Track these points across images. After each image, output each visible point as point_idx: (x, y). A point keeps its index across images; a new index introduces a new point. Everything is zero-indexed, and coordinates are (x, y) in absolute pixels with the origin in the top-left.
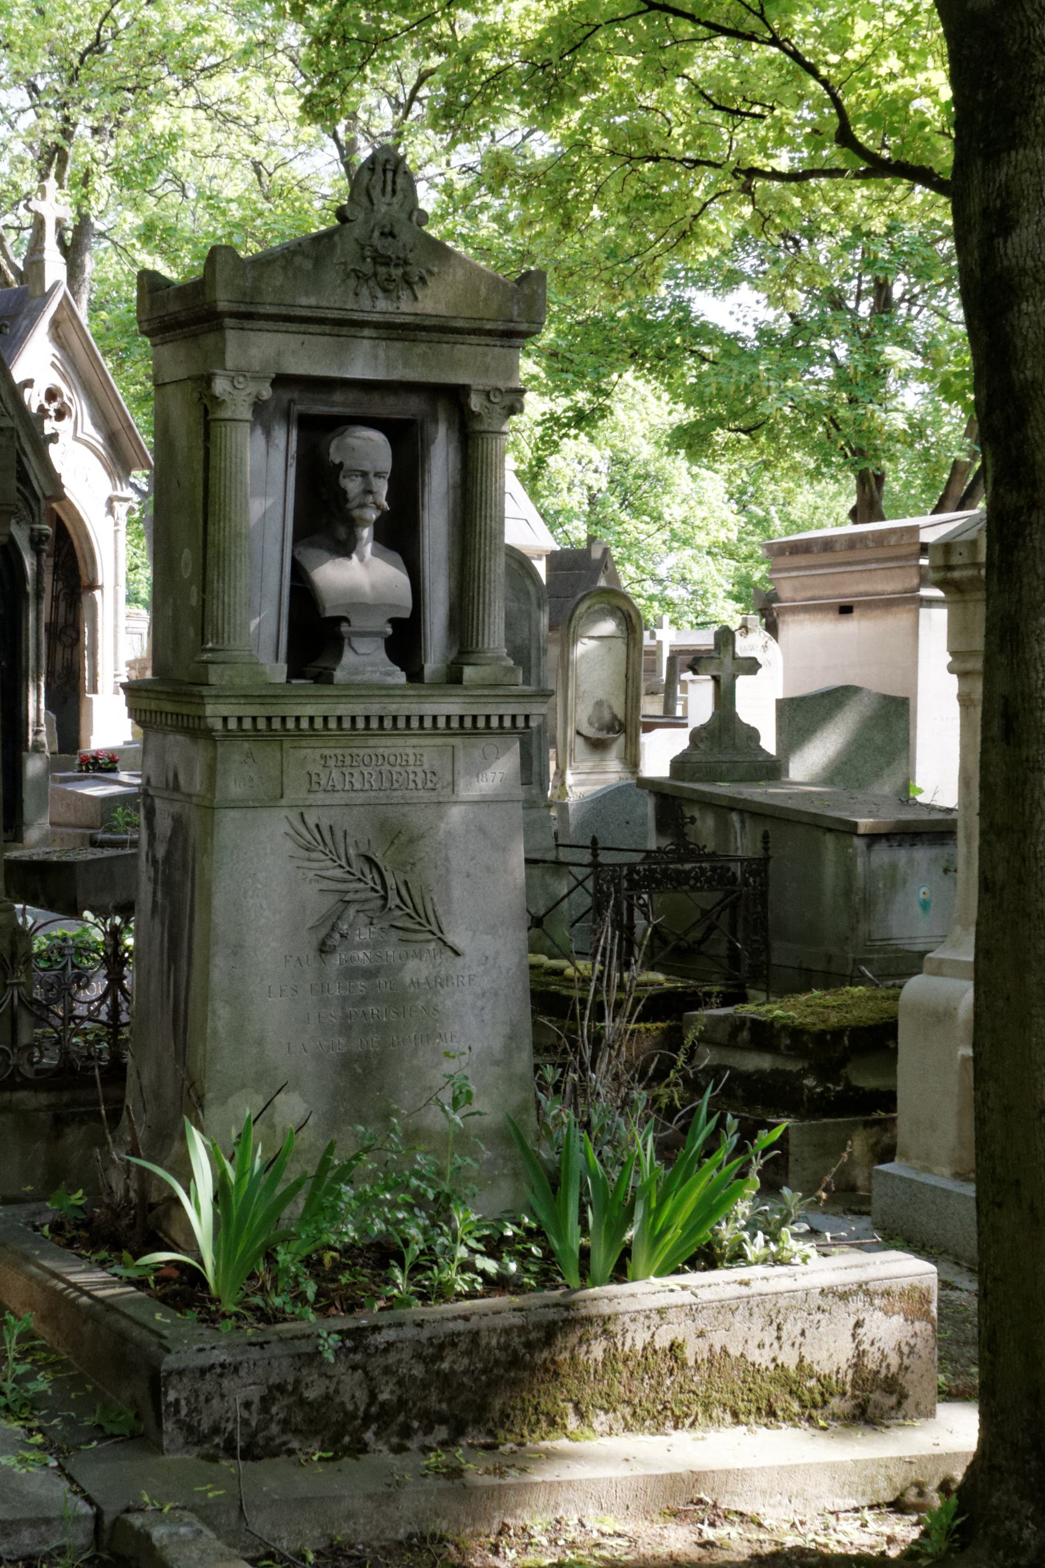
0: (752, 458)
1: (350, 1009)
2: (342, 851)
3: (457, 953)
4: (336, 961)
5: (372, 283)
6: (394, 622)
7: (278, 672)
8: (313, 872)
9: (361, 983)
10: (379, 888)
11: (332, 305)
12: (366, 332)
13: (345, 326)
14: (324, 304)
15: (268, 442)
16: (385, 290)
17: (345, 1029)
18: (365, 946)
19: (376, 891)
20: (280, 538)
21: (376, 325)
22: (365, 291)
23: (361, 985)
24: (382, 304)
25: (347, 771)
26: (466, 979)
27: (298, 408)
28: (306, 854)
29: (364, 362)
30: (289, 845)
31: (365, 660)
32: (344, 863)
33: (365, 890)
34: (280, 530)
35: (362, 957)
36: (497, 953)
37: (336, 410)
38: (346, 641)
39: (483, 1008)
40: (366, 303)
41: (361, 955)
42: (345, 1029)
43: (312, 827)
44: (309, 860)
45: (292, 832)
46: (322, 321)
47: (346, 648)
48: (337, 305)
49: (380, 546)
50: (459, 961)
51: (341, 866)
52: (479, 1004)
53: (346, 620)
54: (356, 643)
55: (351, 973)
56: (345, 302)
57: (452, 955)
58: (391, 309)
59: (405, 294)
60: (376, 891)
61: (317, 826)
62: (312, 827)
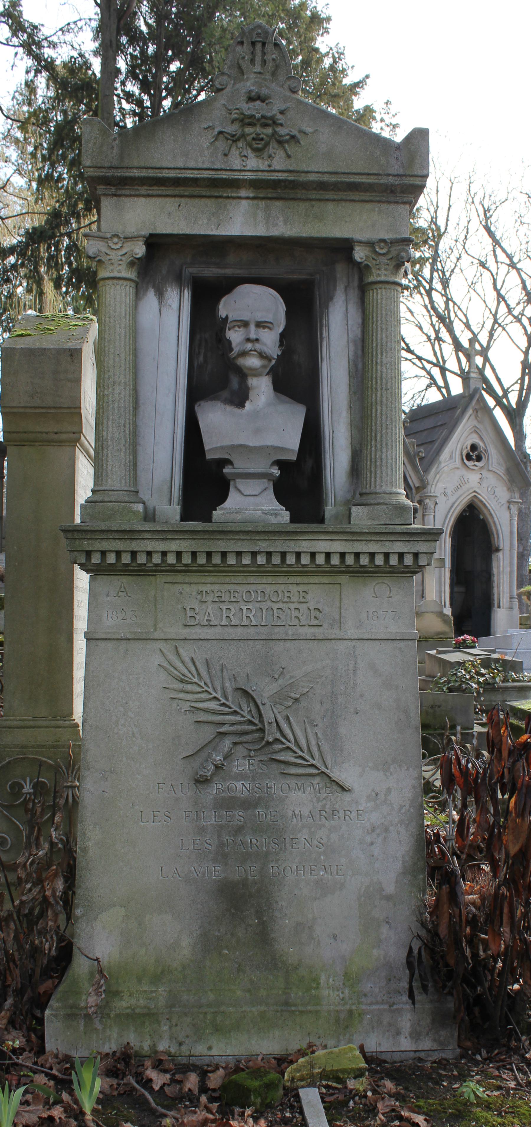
0: (267, 87)
1: (225, 838)
2: (218, 684)
3: (343, 789)
4: (212, 790)
5: (240, 144)
6: (280, 464)
7: (171, 511)
8: (189, 704)
9: (239, 813)
10: (256, 721)
11: (200, 166)
12: (243, 193)
13: (217, 187)
14: (191, 165)
15: (160, 303)
16: (256, 150)
17: (222, 855)
18: (241, 777)
19: (254, 724)
20: (173, 390)
21: (256, 184)
22: (234, 152)
23: (238, 815)
24: (253, 162)
25: (224, 607)
26: (354, 815)
27: (194, 270)
28: (180, 686)
29: (241, 220)
30: (163, 676)
31: (251, 502)
32: (219, 696)
33: (243, 722)
34: (174, 382)
35: (241, 788)
36: (389, 790)
37: (228, 272)
38: (232, 483)
39: (372, 844)
40: (236, 163)
41: (239, 785)
42: (222, 855)
43: (187, 660)
44: (184, 691)
45: (166, 664)
46: (195, 182)
47: (232, 490)
48: (206, 166)
49: (279, 394)
50: (347, 797)
51: (215, 698)
52: (368, 839)
53: (227, 462)
54: (241, 484)
55: (227, 803)
56: (213, 162)
57: (339, 789)
58: (262, 168)
59: (280, 154)
60: (254, 724)
61: (192, 660)
62: (187, 660)
